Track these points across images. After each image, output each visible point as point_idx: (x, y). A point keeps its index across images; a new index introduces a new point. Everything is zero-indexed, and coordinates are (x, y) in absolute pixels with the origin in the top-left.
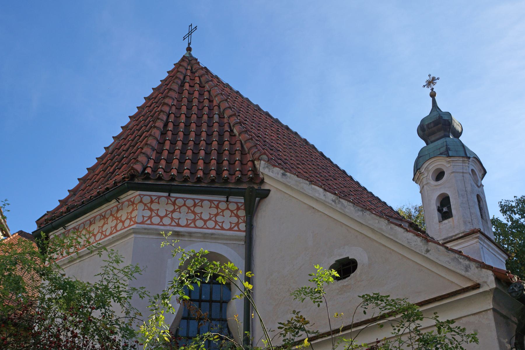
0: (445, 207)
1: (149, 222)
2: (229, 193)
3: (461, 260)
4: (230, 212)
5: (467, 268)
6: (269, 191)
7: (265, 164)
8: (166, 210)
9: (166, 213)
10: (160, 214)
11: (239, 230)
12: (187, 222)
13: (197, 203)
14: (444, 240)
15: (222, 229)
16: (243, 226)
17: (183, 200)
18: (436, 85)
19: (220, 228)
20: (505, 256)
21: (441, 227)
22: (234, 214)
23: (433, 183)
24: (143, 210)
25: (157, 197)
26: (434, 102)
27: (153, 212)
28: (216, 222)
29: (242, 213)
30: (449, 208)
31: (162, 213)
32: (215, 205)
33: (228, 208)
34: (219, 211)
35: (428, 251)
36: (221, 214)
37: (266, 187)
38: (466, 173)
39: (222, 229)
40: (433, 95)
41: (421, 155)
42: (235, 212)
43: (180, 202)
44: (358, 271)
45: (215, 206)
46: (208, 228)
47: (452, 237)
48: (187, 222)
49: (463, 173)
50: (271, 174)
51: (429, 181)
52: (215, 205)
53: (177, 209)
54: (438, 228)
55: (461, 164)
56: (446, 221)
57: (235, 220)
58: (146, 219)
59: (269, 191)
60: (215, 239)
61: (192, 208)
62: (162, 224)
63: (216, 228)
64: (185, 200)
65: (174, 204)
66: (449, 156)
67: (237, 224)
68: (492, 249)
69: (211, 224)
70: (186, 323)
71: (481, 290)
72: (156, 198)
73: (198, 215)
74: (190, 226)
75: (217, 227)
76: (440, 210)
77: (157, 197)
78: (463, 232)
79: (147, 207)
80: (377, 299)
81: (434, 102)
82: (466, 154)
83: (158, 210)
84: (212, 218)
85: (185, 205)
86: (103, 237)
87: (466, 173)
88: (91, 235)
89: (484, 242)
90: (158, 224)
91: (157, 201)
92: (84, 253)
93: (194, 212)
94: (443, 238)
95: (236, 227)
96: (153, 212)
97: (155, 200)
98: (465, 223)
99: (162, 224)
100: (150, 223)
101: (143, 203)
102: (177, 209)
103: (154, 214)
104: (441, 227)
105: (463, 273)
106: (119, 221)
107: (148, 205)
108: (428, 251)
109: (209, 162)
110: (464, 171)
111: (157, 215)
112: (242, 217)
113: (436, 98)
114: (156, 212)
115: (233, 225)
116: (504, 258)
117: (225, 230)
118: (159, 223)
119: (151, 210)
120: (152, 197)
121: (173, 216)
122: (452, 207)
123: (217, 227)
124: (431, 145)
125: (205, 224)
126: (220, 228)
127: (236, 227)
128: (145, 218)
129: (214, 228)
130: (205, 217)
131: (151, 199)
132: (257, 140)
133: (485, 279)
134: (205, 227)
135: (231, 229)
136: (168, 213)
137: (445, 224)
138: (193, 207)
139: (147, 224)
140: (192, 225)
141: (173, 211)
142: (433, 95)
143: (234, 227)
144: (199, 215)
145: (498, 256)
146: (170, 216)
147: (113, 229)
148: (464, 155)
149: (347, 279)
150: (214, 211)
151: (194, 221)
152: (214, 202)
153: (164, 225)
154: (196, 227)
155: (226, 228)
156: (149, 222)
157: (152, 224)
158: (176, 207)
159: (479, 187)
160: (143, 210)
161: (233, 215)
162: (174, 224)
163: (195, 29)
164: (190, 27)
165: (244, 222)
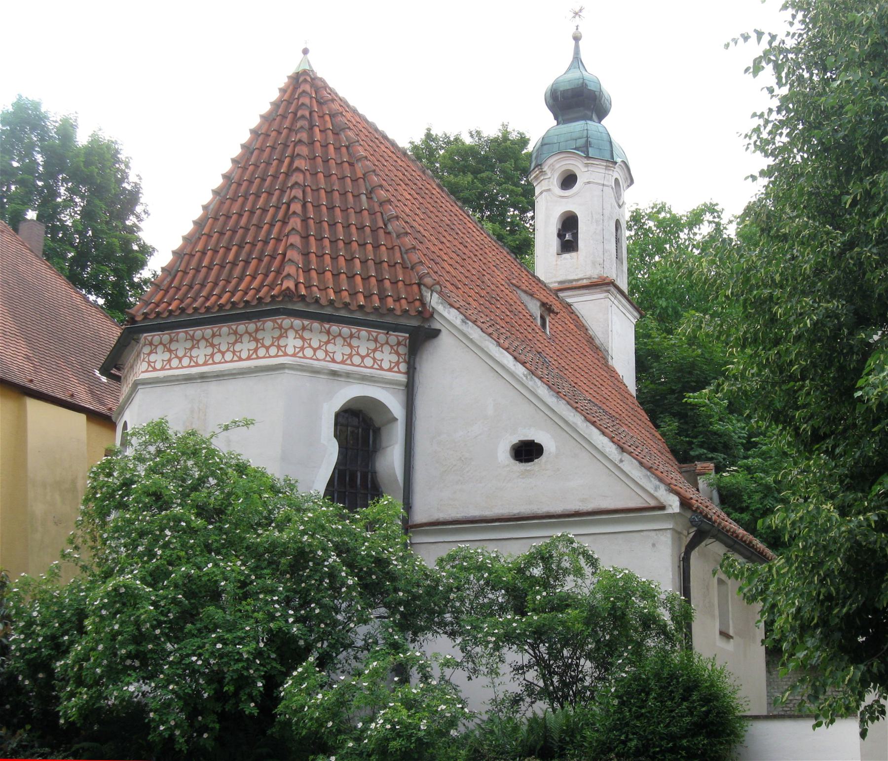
0: (568, 232)
1: (301, 354)
2: (390, 328)
3: (652, 479)
5: (656, 488)
6: (440, 331)
8: (320, 341)
11: (399, 372)
14: (560, 283)
16: (403, 367)
20: (636, 314)
21: (559, 263)
23: (557, 190)
29: (402, 350)
30: (575, 236)
33: (387, 343)
35: (621, 461)
37: (436, 326)
38: (607, 186)
39: (381, 368)
41: (546, 141)
44: (543, 458)
46: (366, 367)
47: (571, 281)
49: (603, 185)
50: (445, 314)
51: (551, 187)
54: (554, 263)
55: (603, 171)
56: (567, 256)
57: (394, 358)
59: (440, 331)
60: (375, 381)
66: (588, 157)
67: (397, 364)
68: (623, 306)
71: (666, 512)
76: (561, 235)
78: (589, 278)
82: (612, 157)
86: (236, 358)
87: (607, 186)
88: (216, 350)
89: (616, 297)
90: (311, 358)
93: (350, 345)
94: (559, 279)
98: (594, 263)
103: (306, 345)
104: (559, 263)
105: (652, 492)
106: (259, 345)
108: (621, 461)
110: (606, 183)
113: (580, 42)
116: (635, 317)
122: (580, 236)
124: (561, 126)
129: (372, 367)
133: (671, 503)
135: (390, 370)
137: (565, 259)
141: (193, 347)
142: (577, 39)
145: (627, 314)
147: (251, 352)
148: (608, 157)
149: (530, 464)
151: (350, 356)
153: (318, 360)
154: (353, 365)
157: (305, 357)
159: (620, 206)
165: (405, 361)
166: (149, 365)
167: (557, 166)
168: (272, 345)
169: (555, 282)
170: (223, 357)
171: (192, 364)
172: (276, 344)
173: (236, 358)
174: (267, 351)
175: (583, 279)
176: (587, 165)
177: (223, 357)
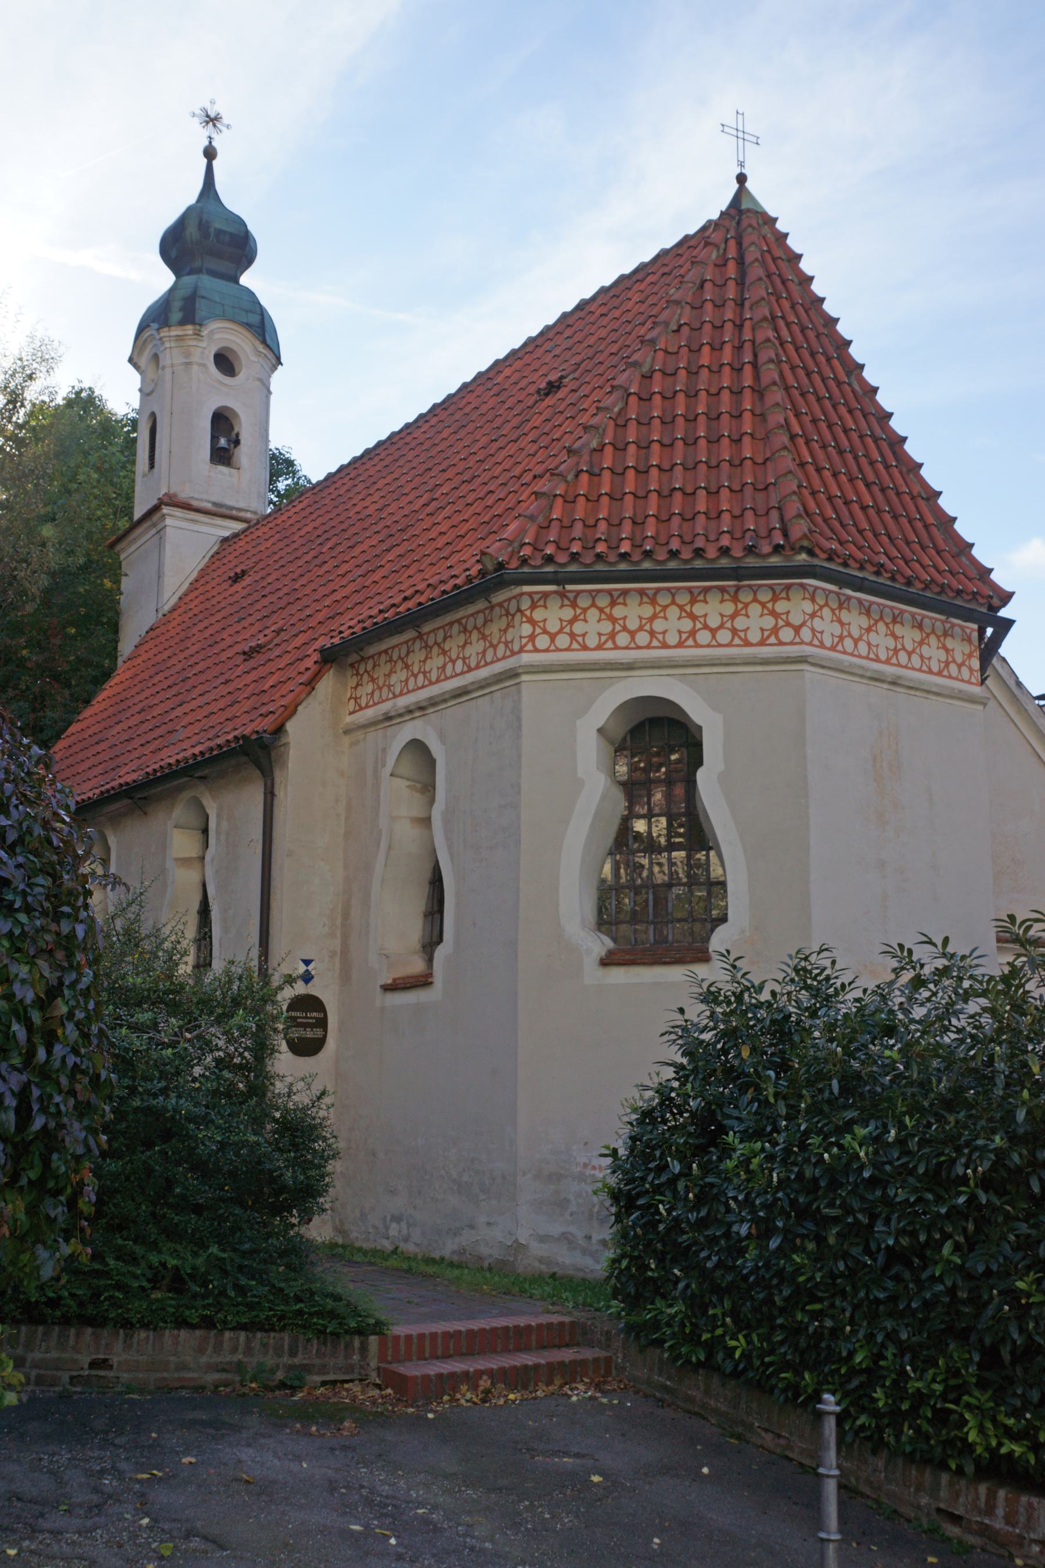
7: (309, 482)
12: (680, 637)
18: (201, 105)
19: (741, 643)
28: (652, 633)
31: (553, 627)
34: (579, 611)
36: (743, 612)
40: (210, 153)
42: (688, 608)
47: (232, 508)
70: (187, 855)
74: (768, 642)
79: (686, 612)
95: (530, 644)
101: (760, 602)
111: (545, 632)
113: (215, 163)
114: (702, 620)
115: (603, 638)
117: (751, 645)
123: (737, 641)
126: (741, 643)
127: (530, 644)
130: (796, 619)
134: (797, 640)
136: (644, 621)
137: (221, 472)
140: (530, 647)
142: (210, 153)
143: (606, 641)
146: (647, 627)
156: (690, 642)
161: (766, 612)
162: (816, 642)
163: (740, 117)
164: (726, 129)
166: (814, 635)
167: (217, 336)
168: (641, 628)
169: (209, 502)
170: (714, 637)
171: (872, 656)
172: (647, 627)
173: (655, 643)
174: (633, 639)
175: (247, 511)
176: (259, 353)
177: (714, 637)
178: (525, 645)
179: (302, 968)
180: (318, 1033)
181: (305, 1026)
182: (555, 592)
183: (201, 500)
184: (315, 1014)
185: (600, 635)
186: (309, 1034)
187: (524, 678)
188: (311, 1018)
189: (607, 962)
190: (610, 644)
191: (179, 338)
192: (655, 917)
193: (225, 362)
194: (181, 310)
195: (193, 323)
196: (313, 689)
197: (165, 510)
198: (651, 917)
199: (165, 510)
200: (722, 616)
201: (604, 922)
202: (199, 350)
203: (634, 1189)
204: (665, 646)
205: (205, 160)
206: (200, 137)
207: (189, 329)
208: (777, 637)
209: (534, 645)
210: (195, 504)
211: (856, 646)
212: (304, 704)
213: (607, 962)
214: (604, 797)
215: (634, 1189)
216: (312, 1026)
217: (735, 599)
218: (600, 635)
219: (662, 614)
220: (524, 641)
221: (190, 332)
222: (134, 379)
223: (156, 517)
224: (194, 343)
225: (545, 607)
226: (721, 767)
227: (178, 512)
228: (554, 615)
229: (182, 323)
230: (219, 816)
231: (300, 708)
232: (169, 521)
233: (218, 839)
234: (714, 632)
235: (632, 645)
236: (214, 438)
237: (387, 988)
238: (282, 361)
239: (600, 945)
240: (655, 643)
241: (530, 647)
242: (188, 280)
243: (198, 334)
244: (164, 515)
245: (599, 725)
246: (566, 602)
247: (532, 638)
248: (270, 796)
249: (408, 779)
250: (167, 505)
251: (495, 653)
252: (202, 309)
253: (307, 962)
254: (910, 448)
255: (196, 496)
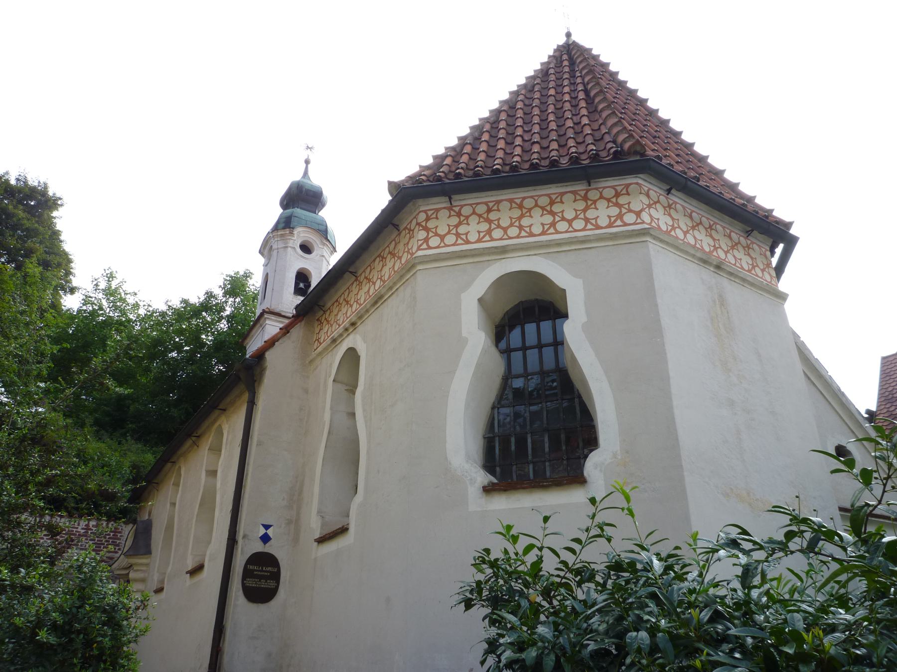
4: (540, 211)
9: (449, 228)
10: (632, 207)
13: (619, 191)
15: (598, 227)
17: (532, 200)
22: (484, 218)
24: (541, 216)
25: (557, 195)
26: (307, 168)
27: (556, 216)
28: (521, 228)
31: (442, 230)
32: (581, 196)
36: (465, 222)
40: (307, 162)
43: (528, 203)
45: (455, 214)
48: (610, 220)
52: (581, 196)
53: (463, 221)
58: (546, 227)
61: (548, 208)
62: (572, 230)
63: (458, 242)
64: (536, 198)
65: (459, 214)
69: (451, 239)
72: (623, 189)
73: (495, 222)
74: (614, 225)
75: (523, 234)
77: (557, 195)
80: (353, 324)
81: (307, 168)
83: (563, 212)
84: (515, 222)
85: (536, 205)
91: (624, 192)
92: (728, 269)
93: (617, 205)
96: (556, 216)
97: (555, 199)
99: (572, 230)
100: (621, 224)
101: (605, 199)
102: (463, 221)
106: (557, 219)
107: (612, 200)
109: (565, 143)
112: (495, 220)
113: (309, 166)
114: (496, 222)
117: (602, 228)
118: (440, 244)
119: (490, 221)
120: (552, 196)
121: (426, 234)
123: (460, 241)
125: (570, 225)
126: (593, 227)
128: (545, 226)
130: (569, 215)
131: (616, 191)
132: (621, 113)
134: (639, 221)
136: (514, 220)
138: (615, 198)
139: (617, 226)
141: (522, 216)
142: (307, 162)
144: (434, 230)
150: (517, 213)
152: (516, 200)
155: (604, 225)
156: (487, 238)
158: (462, 218)
160: (541, 216)
168: (512, 225)
176: (324, 244)
178: (421, 245)
179: (262, 531)
180: (271, 584)
181: (261, 578)
182: (444, 208)
183: (287, 312)
184: (269, 569)
185: (479, 232)
186: (263, 584)
187: (419, 267)
188: (266, 571)
189: (488, 490)
190: (487, 238)
191: (282, 235)
192: (534, 456)
193: (306, 248)
194: (284, 223)
195: (290, 228)
196: (288, 332)
197: (266, 316)
198: (530, 458)
199: (266, 316)
200: (576, 210)
201: (489, 465)
202: (292, 241)
203: (257, 571)
204: (532, 235)
205: (305, 165)
206: (305, 154)
207: (287, 231)
208: (622, 221)
209: (428, 245)
210: (283, 314)
211: (685, 236)
212: (280, 341)
213: (488, 490)
214: (484, 352)
215: (257, 571)
216: (266, 578)
217: (585, 198)
218: (479, 232)
219: (528, 214)
220: (420, 242)
221: (288, 232)
222: (262, 260)
223: (261, 321)
224: (290, 237)
225: (437, 218)
226: (584, 319)
227: (273, 317)
228: (443, 223)
229: (284, 228)
230: (228, 432)
231: (276, 343)
232: (267, 322)
233: (226, 448)
234: (570, 222)
235: (505, 237)
236: (297, 284)
237: (321, 540)
238: (337, 249)
239: (483, 478)
240: (523, 234)
241: (425, 246)
242: (289, 211)
243: (291, 233)
244: (266, 318)
245: (479, 296)
246: (453, 213)
247: (426, 240)
248: (252, 404)
249: (347, 385)
250: (267, 313)
251: (401, 262)
252: (294, 222)
253: (267, 527)
254: (697, 148)
255: (284, 310)
